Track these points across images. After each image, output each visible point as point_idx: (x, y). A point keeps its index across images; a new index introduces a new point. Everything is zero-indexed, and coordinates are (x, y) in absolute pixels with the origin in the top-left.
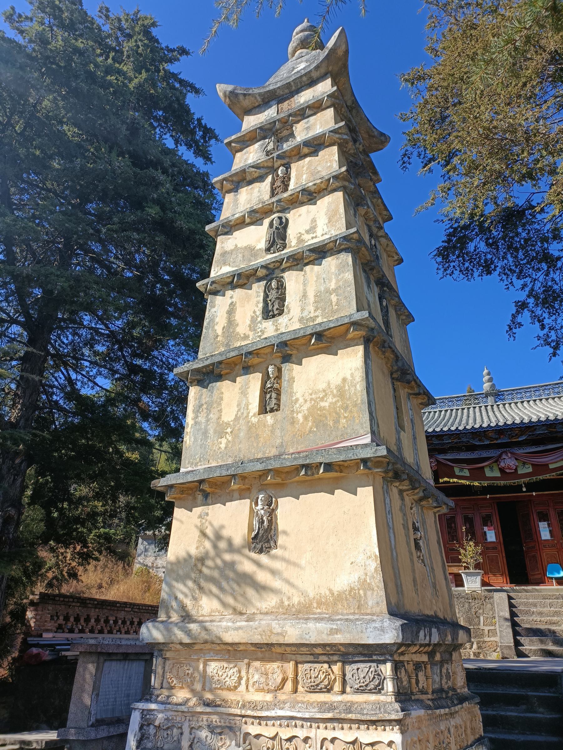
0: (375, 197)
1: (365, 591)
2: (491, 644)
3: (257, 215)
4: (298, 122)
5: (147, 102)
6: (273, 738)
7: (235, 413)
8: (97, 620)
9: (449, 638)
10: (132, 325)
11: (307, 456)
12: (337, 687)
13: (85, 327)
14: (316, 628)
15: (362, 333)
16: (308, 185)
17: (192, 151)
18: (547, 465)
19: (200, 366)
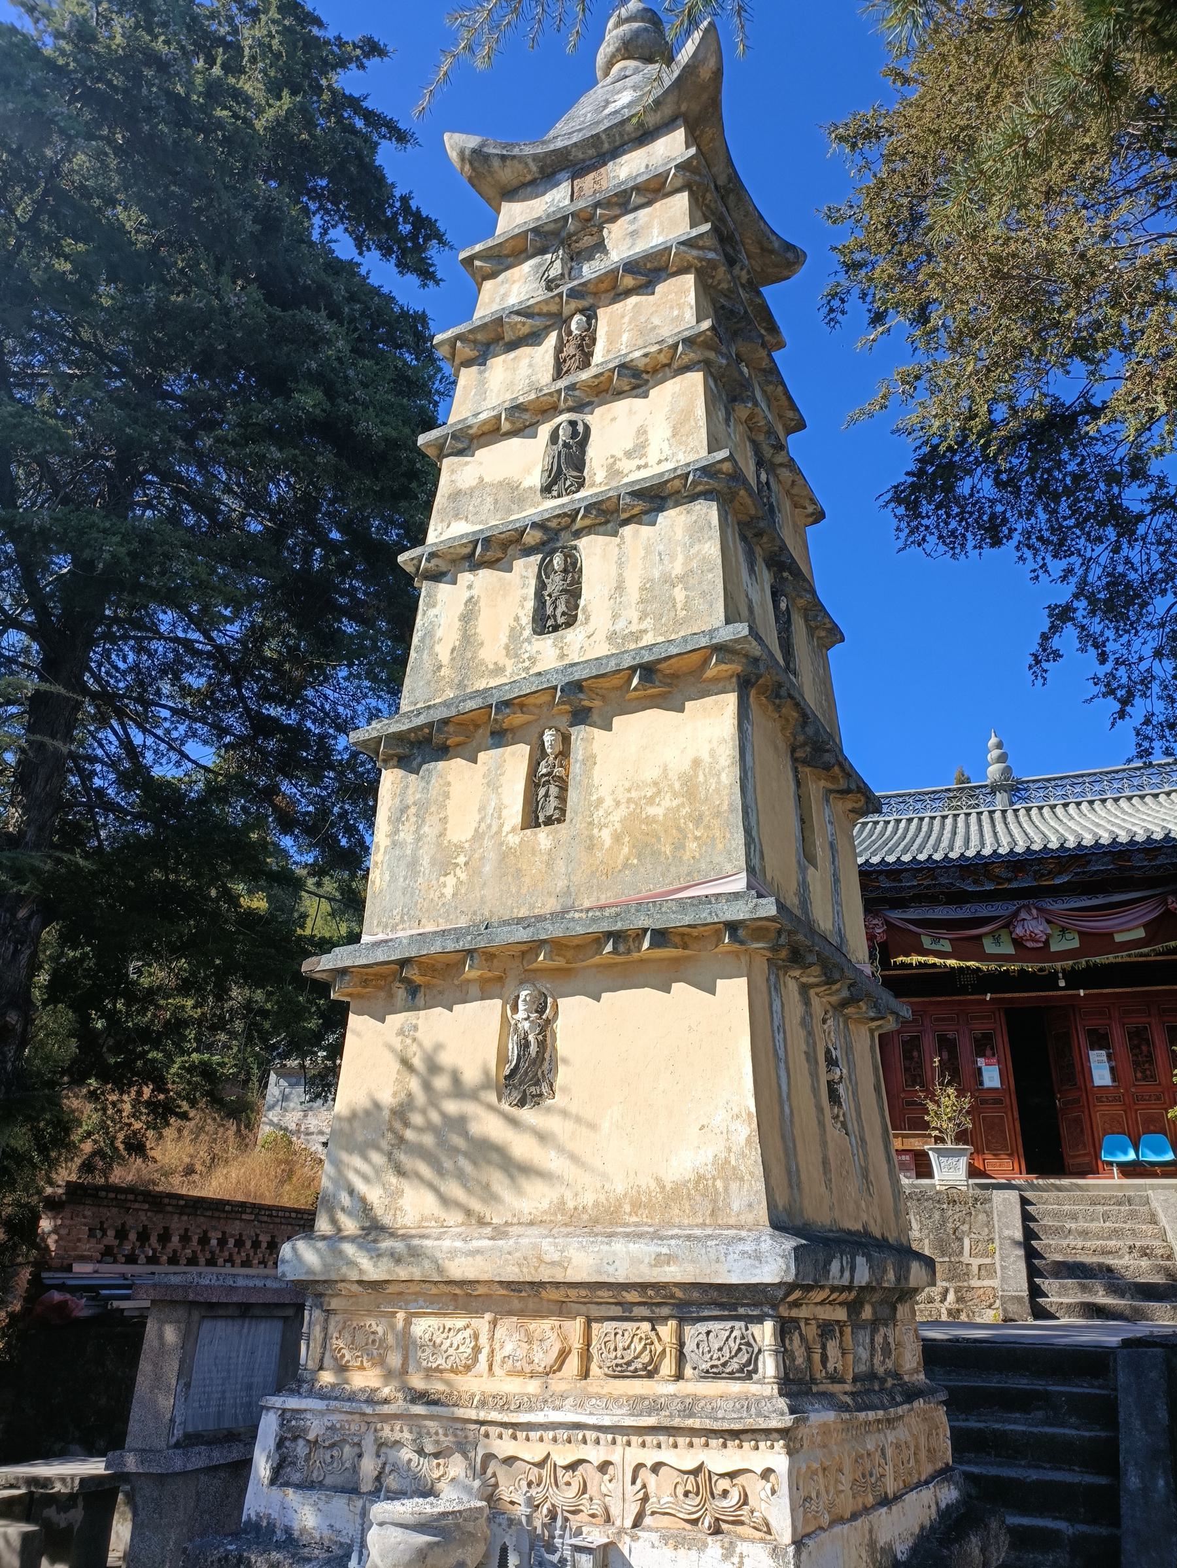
0: (770, 383)
1: (726, 1181)
2: (980, 1287)
3: (526, 416)
4: (614, 219)
5: (293, 158)
6: (541, 1465)
7: (475, 825)
8: (185, 1239)
9: (891, 1275)
10: (257, 635)
11: (618, 915)
12: (667, 1367)
13: (161, 637)
14: (628, 1253)
15: (735, 667)
16: (632, 356)
17: (393, 261)
18: (1111, 935)
19: (404, 728)
